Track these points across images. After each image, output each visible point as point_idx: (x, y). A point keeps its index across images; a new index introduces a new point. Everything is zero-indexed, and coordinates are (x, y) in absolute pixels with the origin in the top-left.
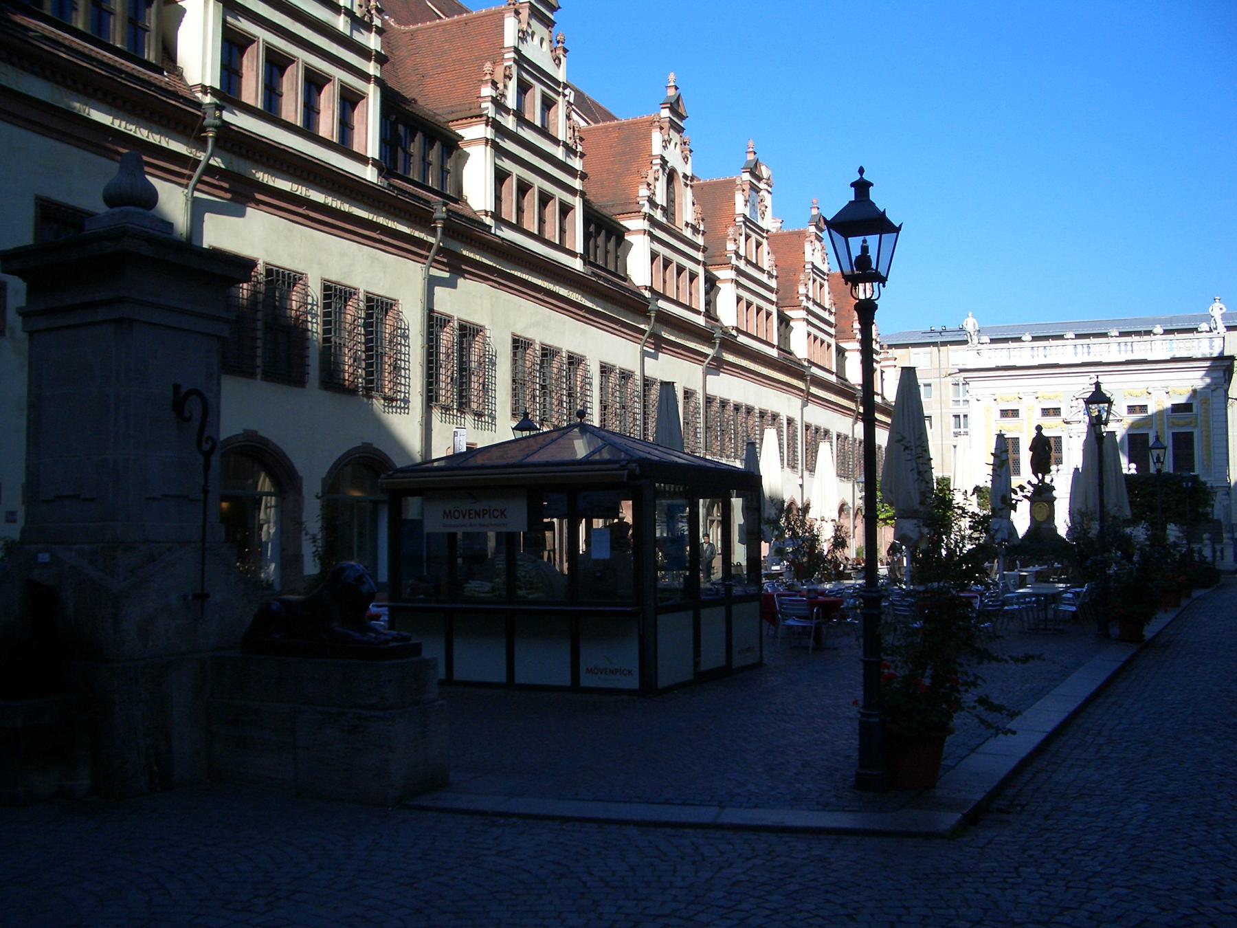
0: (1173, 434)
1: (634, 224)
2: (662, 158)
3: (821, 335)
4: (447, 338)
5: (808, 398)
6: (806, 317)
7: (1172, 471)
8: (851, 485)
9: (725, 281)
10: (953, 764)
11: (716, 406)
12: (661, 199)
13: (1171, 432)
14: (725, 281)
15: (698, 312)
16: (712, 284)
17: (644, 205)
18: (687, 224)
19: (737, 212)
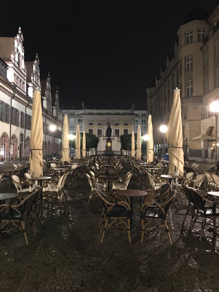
0: (89, 129)
1: (10, 65)
2: (17, 49)
3: (49, 104)
4: (28, 118)
5: (13, 97)
6: (13, 67)
7: (88, 133)
8: (24, 130)
9: (10, 67)
10: (3, 282)
11: (28, 116)
12: (17, 59)
13: (89, 123)
14: (10, 67)
15: (25, 92)
16: (28, 86)
17: (12, 60)
18: (23, 69)
19: (34, 70)
